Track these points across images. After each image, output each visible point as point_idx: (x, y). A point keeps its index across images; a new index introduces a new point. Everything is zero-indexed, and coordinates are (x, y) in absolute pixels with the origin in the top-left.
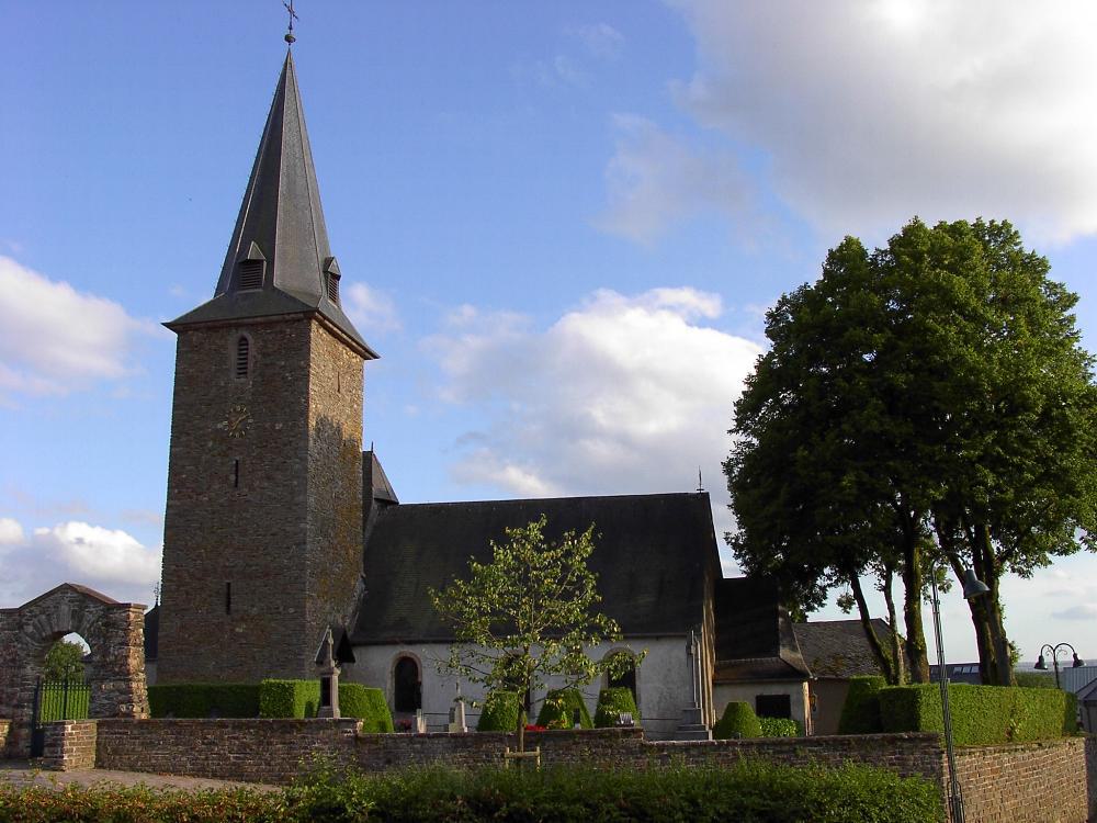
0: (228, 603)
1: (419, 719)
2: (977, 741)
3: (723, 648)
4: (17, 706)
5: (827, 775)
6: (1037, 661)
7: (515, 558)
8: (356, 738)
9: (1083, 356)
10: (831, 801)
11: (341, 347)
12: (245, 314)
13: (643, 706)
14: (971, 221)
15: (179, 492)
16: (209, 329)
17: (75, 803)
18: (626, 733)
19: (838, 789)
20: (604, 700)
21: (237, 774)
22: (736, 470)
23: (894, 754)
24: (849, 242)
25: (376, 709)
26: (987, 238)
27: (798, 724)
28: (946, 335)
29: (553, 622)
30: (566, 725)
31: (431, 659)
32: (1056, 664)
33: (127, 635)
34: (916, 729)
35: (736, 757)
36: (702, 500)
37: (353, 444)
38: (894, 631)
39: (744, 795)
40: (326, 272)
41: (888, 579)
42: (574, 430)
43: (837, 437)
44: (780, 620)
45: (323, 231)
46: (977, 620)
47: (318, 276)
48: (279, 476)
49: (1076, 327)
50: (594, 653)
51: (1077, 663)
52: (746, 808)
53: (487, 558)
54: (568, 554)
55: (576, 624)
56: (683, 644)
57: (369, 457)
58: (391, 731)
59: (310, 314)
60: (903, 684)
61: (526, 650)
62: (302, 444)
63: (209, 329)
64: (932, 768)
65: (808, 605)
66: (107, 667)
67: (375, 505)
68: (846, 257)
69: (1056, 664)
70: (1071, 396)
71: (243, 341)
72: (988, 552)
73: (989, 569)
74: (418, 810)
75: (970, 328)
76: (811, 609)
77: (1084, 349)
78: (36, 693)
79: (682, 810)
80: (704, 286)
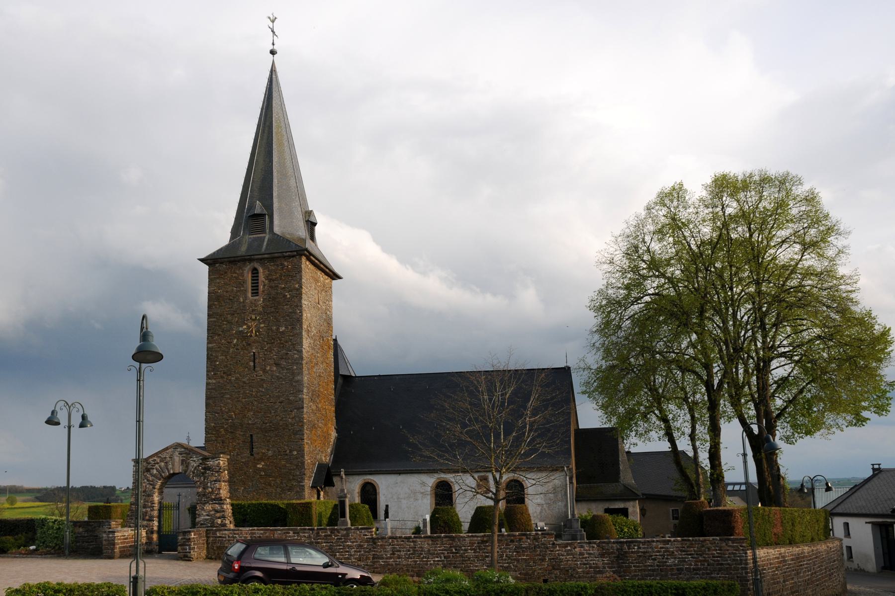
11: (319, 273)
16: (230, 262)
31: (388, 487)
48: (283, 363)
71: (255, 272)
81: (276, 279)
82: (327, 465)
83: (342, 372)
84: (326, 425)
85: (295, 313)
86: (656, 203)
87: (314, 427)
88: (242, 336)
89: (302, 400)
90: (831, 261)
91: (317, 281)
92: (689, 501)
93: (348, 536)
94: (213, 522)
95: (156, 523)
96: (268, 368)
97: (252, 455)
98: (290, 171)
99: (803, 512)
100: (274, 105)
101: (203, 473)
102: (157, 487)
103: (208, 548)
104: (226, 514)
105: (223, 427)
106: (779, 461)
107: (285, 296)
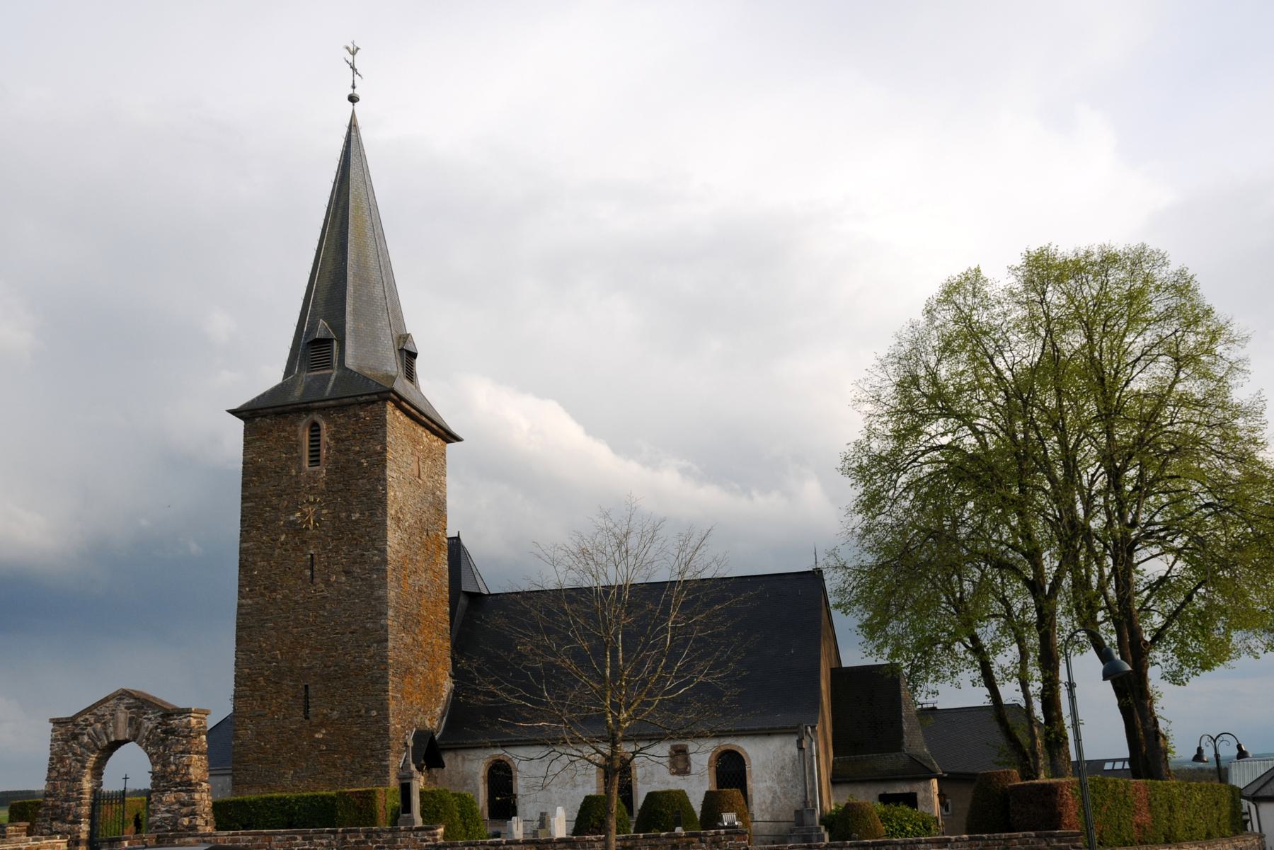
3: (842, 744)
6: (1236, 752)
11: (420, 430)
16: (277, 414)
31: (528, 766)
40: (401, 350)
48: (357, 570)
56: (795, 739)
57: (455, 545)
59: (384, 395)
60: (1043, 779)
63: (277, 414)
69: (1217, 756)
71: (315, 428)
81: (347, 439)
82: (432, 734)
83: (467, 586)
84: (432, 669)
85: (376, 490)
86: (939, 301)
87: (408, 671)
88: (295, 530)
89: (385, 628)
90: (1219, 381)
91: (416, 442)
92: (1013, 780)
93: (396, 842)
94: (176, 824)
95: (85, 827)
96: (333, 578)
97: (307, 718)
98: (375, 275)
99: (1189, 788)
100: (352, 175)
101: (163, 740)
102: (90, 764)
104: (198, 809)
105: (262, 675)
106: (1158, 712)
107: (360, 464)
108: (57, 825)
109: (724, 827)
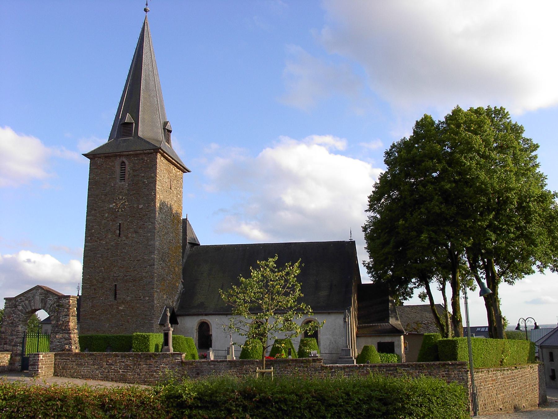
0: (116, 294)
1: (211, 353)
2: (485, 366)
3: (360, 318)
4: (14, 346)
5: (411, 381)
7: (262, 275)
8: (182, 362)
9: (541, 175)
10: (414, 394)
11: (172, 166)
12: (123, 150)
13: (321, 347)
14: (485, 108)
15: (91, 239)
16: (106, 157)
17: (56, 393)
18: (314, 361)
19: (417, 388)
20: (303, 343)
21: (123, 380)
22: (368, 230)
23: (445, 371)
24: (426, 117)
25: (190, 350)
26: (493, 116)
27: (398, 356)
28: (470, 165)
29: (280, 307)
30: (284, 356)
31: (217, 324)
32: (526, 327)
33: (68, 311)
34: (455, 359)
35: (368, 373)
36: (352, 244)
37: (178, 215)
38: (446, 311)
39: (372, 391)
40: (164, 129)
41: (444, 284)
42: (275, 206)
43: (419, 215)
44: (390, 304)
45: (162, 108)
46: (488, 305)
47: (161, 131)
48: (141, 231)
49: (537, 161)
50: (298, 321)
51: (536, 327)
52: (373, 397)
53: (248, 275)
54: (288, 274)
55: (291, 308)
57: (185, 221)
58: (197, 359)
59: (157, 150)
60: (450, 338)
61: (267, 320)
62: (152, 215)
63: (106, 157)
64: (463, 379)
65: (404, 297)
66: (56, 324)
67: (188, 246)
68: (424, 127)
69: (526, 327)
70: (533, 197)
71: (123, 163)
72: (493, 272)
73: (493, 282)
74: (217, 397)
75: (483, 161)
76: (406, 299)
77: (541, 173)
78: (23, 340)
79: (342, 398)
80: (336, 134)
85: (151, 195)
91: (170, 172)
96: (130, 235)
103: (55, 367)
108: (8, 347)
109: (311, 357)
